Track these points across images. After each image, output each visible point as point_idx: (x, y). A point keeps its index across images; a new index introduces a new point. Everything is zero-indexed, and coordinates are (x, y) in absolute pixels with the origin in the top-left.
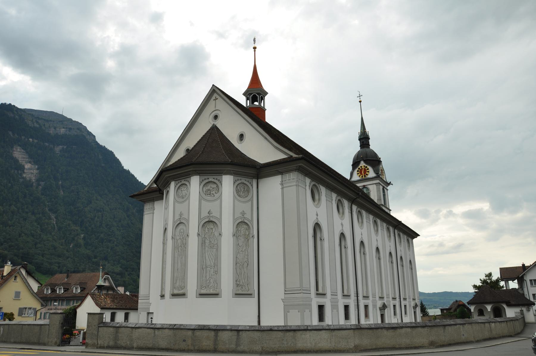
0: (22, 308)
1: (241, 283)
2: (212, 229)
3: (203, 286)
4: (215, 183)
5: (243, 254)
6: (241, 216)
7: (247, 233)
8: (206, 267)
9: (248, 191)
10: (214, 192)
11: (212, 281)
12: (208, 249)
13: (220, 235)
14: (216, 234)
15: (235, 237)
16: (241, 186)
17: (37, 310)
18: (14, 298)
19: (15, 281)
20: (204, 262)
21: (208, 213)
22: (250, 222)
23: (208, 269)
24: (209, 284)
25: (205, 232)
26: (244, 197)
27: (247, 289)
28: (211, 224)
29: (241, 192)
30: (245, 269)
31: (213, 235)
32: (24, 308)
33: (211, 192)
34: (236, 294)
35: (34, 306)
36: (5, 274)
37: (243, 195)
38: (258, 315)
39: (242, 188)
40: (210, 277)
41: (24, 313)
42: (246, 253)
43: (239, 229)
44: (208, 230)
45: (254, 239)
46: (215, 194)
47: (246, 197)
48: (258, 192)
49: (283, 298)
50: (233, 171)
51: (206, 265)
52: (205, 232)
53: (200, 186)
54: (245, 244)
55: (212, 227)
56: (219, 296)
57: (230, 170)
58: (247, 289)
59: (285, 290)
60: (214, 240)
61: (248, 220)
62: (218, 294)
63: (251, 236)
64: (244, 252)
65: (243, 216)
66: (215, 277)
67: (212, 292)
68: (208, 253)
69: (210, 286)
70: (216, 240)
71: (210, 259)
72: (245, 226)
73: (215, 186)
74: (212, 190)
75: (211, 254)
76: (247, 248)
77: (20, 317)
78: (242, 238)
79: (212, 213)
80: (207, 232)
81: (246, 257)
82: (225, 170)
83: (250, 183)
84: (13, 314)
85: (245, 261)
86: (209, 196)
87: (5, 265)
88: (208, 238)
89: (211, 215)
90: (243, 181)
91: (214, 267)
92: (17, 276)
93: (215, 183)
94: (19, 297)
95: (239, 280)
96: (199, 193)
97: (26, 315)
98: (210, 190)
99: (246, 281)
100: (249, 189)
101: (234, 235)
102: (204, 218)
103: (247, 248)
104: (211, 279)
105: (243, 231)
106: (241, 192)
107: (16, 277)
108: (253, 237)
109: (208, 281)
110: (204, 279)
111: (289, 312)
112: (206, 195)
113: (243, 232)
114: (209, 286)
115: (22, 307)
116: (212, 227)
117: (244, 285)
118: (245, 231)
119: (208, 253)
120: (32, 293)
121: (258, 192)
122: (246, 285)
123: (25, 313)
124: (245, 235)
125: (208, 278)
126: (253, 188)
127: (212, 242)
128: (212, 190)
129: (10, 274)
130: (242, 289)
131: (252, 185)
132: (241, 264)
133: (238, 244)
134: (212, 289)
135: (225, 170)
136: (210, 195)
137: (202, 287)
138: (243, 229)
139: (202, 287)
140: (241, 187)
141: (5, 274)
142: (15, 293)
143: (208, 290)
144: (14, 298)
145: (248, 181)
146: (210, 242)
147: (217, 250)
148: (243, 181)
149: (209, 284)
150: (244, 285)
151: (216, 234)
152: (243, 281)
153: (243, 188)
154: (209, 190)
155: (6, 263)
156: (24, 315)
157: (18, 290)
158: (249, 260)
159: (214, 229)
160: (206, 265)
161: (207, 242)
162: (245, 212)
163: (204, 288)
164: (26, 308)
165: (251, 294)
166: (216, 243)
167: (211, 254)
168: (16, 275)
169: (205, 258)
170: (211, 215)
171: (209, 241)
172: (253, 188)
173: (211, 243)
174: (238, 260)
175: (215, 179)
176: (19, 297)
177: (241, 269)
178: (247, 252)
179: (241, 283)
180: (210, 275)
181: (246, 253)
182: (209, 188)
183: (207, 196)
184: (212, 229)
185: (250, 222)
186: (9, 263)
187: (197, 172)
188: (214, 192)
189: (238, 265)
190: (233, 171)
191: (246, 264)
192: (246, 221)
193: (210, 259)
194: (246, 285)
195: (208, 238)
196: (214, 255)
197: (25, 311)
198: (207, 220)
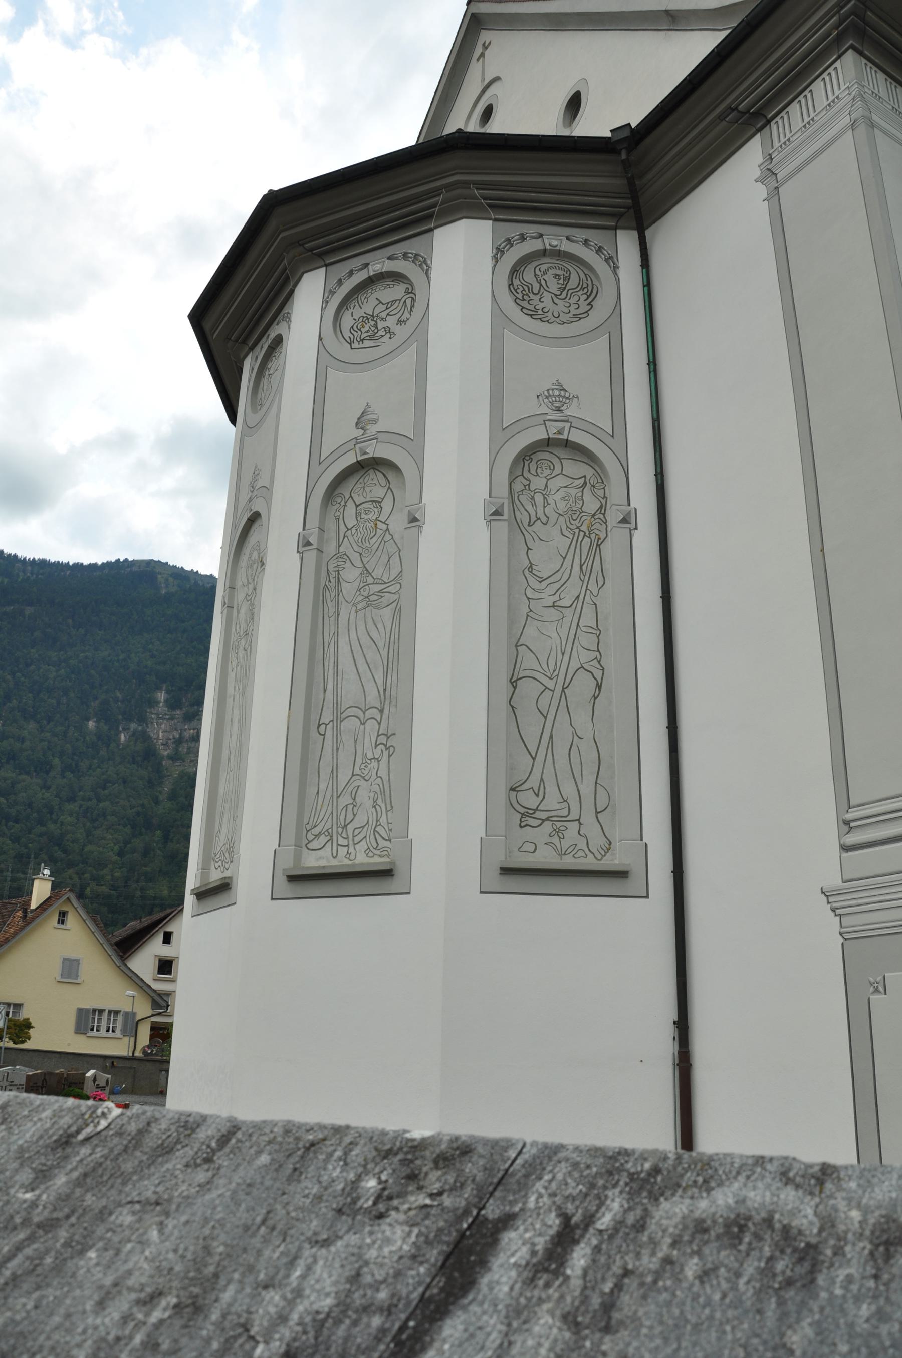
0: (87, 1010)
1: (552, 802)
2: (378, 502)
3: (316, 831)
4: (396, 277)
5: (567, 621)
6: (544, 410)
7: (591, 505)
8: (339, 717)
9: (592, 294)
10: (391, 322)
11: (364, 796)
12: (353, 614)
13: (414, 519)
14: (398, 523)
15: (502, 527)
16: (543, 267)
17: (138, 1018)
18: (59, 979)
19: (61, 926)
20: (330, 686)
21: (357, 424)
22: (608, 440)
23: (350, 724)
24: (350, 817)
25: (342, 526)
26: (564, 317)
27: (597, 841)
28: (374, 478)
29: (547, 297)
30: (581, 718)
31: (379, 532)
32: (94, 1011)
33: (381, 324)
34: (506, 871)
35: (125, 1006)
36: (33, 906)
37: (556, 310)
38: (672, 1014)
39: (549, 277)
40: (357, 771)
41: (96, 1025)
42: (588, 619)
43: (538, 483)
44: (358, 515)
45: (636, 534)
46: (396, 328)
47: (578, 317)
48: (648, 285)
49: (834, 881)
50: (480, 185)
51: (337, 704)
52: (342, 526)
53: (323, 309)
54: (576, 567)
55: (379, 492)
56: (394, 884)
57: (465, 184)
58: (597, 841)
59: (847, 823)
60: (385, 559)
61: (592, 430)
62: (386, 873)
63: (613, 516)
64: (568, 613)
65: (558, 410)
66: (383, 773)
67: (362, 859)
68: (353, 635)
69: (356, 823)
70: (395, 560)
71: (363, 668)
72: (576, 468)
73: (397, 291)
74: (384, 315)
75: (365, 640)
76: (593, 587)
77: (82, 1038)
78: (555, 532)
79: (375, 422)
80: (351, 522)
81: (587, 640)
82: (436, 192)
83: (599, 250)
84: (30, 1024)
85: (575, 665)
86: (367, 343)
87: (34, 877)
88: (355, 557)
89: (372, 430)
90: (555, 238)
91: (382, 711)
92: (67, 912)
93: (396, 277)
94: (77, 976)
95: (534, 782)
96: (320, 339)
97: (103, 1032)
98: (372, 316)
99: (587, 789)
100: (596, 282)
101: (496, 513)
102: (339, 452)
103: (593, 587)
104: (362, 783)
105: (562, 493)
106: (547, 297)
107: (63, 915)
108: (625, 520)
109: (346, 800)
110: (323, 787)
111: (881, 987)
112: (356, 345)
113: (563, 499)
114: (350, 828)
115: (88, 1007)
116: (379, 492)
117: (574, 815)
118: (573, 491)
119: (353, 635)
120: (118, 967)
121: (648, 285)
122: (588, 818)
123: (98, 1027)
124: (574, 513)
125: (344, 776)
126: (616, 274)
127: (377, 573)
128: (384, 315)
129: (44, 906)
130: (555, 840)
131: (612, 261)
132: (550, 684)
133: (531, 568)
134: (363, 846)
135: (436, 192)
136: (371, 338)
137: (310, 837)
138: (560, 481)
139: (310, 837)
140: (545, 273)
141: (33, 906)
142: (63, 963)
143: (343, 851)
144: (59, 979)
145: (586, 242)
146: (366, 572)
147: (397, 612)
148: (555, 243)
149: (350, 817)
150: (574, 815)
151: (398, 523)
152: (569, 789)
153: (556, 276)
154: (366, 318)
155: (37, 871)
156: (98, 1030)
157: (73, 955)
158: (610, 662)
159: (387, 505)
160: (337, 704)
161: (350, 574)
162: (572, 389)
163: (323, 839)
164: (101, 1012)
165: (622, 875)
166: (394, 573)
167: (365, 640)
168: (65, 909)
169: (336, 664)
170: (372, 430)
171: (357, 572)
172: (622, 273)
173: (370, 580)
174: (528, 662)
175: (397, 258)
176: (77, 976)
177: (550, 717)
178: (588, 611)
179: (552, 802)
180: (359, 761)
181: (588, 619)
182: (368, 308)
183: (361, 345)
184: (378, 502)
185: (608, 440)
186: (47, 872)
187: (311, 250)
188: (391, 322)
189: (528, 688)
190: (480, 185)
191: (583, 685)
192: (576, 437)
193: (363, 668)
194: (588, 818)
195: (355, 557)
196: (380, 644)
197: (99, 1019)
198: (350, 459)
